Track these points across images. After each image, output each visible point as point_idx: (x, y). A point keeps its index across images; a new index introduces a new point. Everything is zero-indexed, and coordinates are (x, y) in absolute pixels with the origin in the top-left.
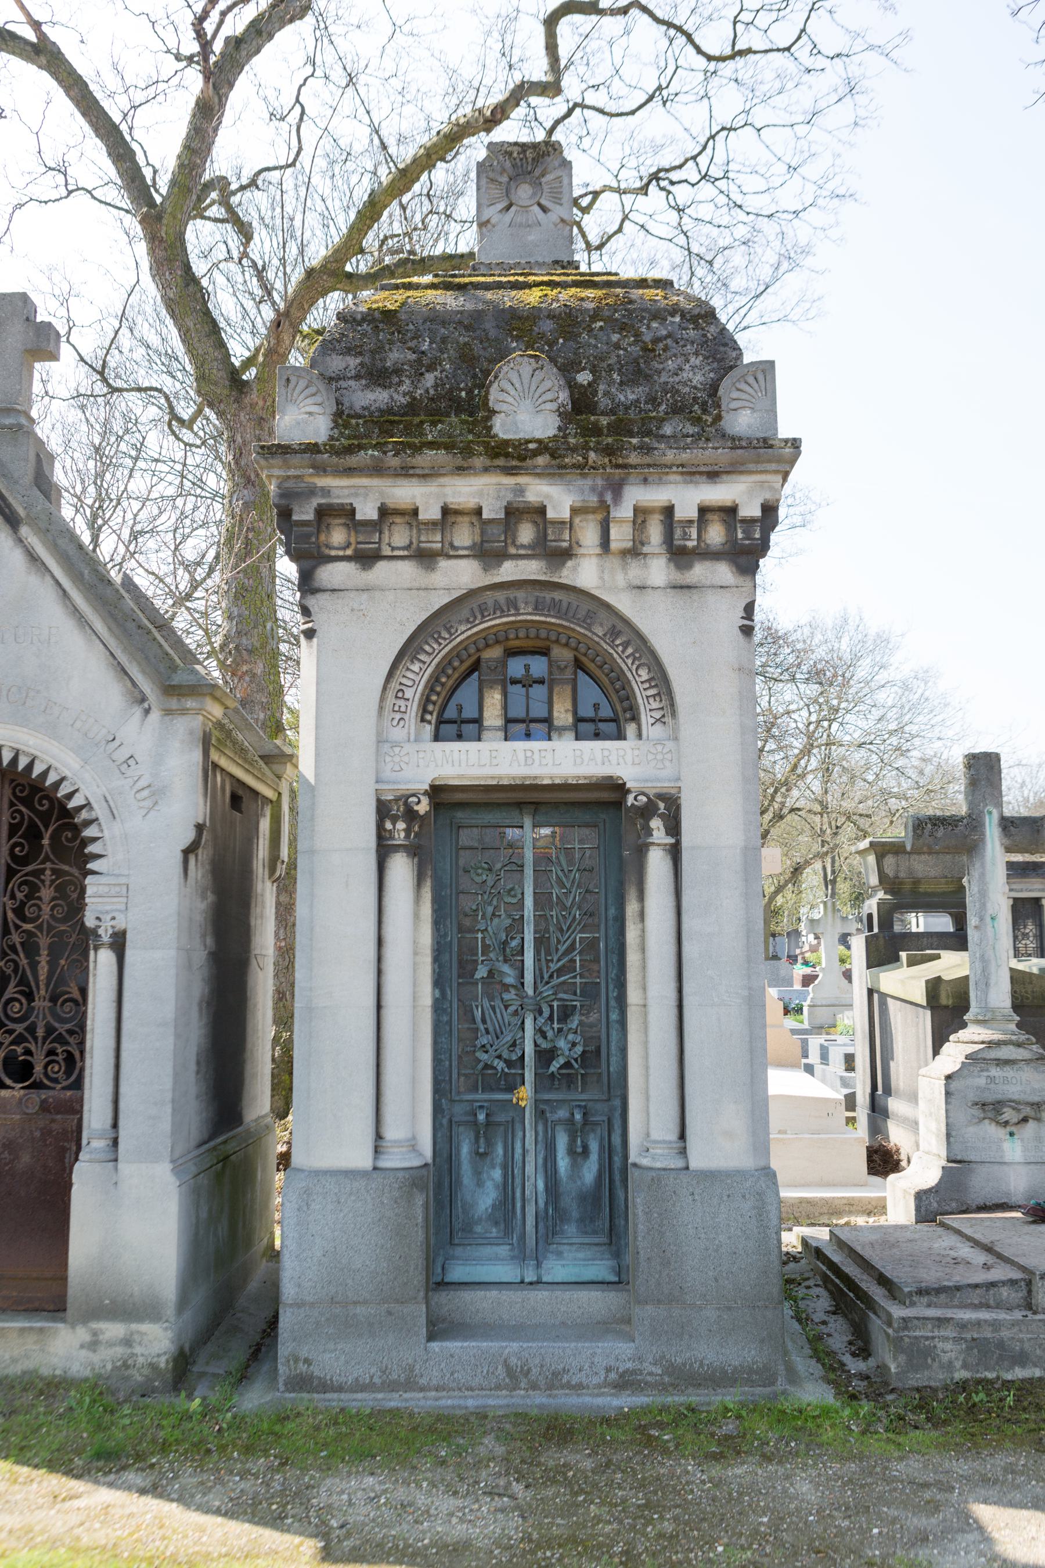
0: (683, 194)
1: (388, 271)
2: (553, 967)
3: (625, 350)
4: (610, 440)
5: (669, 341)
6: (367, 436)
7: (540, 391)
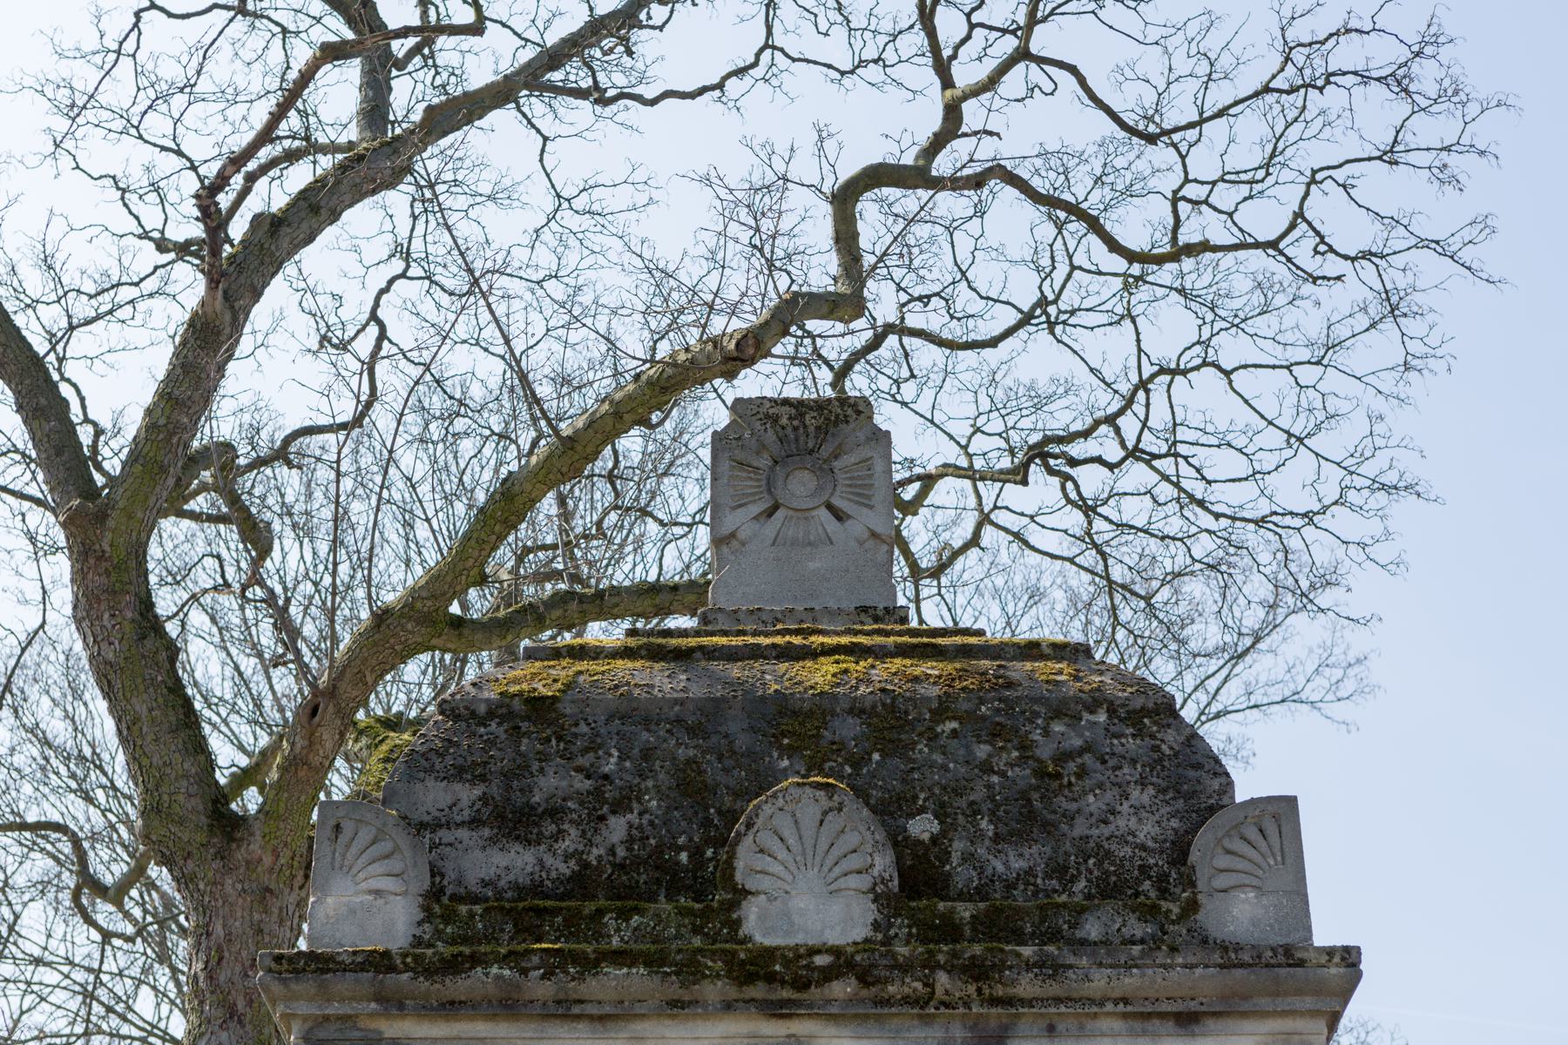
0: (1091, 480)
1: (534, 616)
3: (1003, 774)
4: (977, 949)
5: (1087, 759)
6: (489, 938)
7: (836, 852)
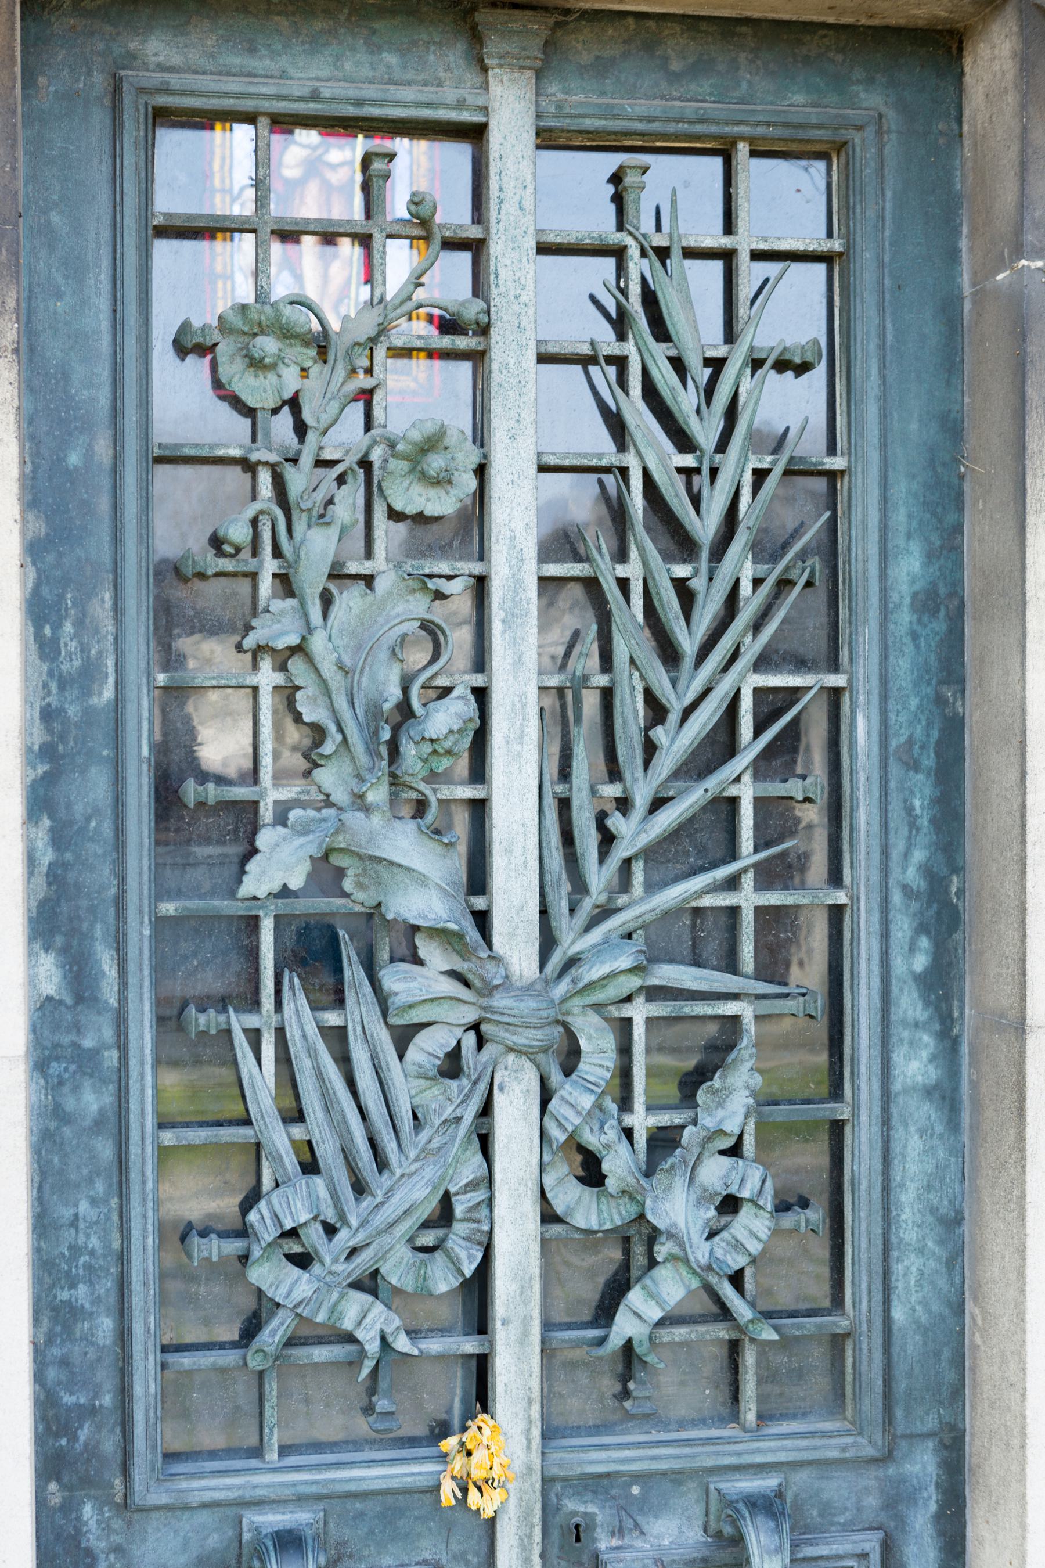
2: (634, 833)
